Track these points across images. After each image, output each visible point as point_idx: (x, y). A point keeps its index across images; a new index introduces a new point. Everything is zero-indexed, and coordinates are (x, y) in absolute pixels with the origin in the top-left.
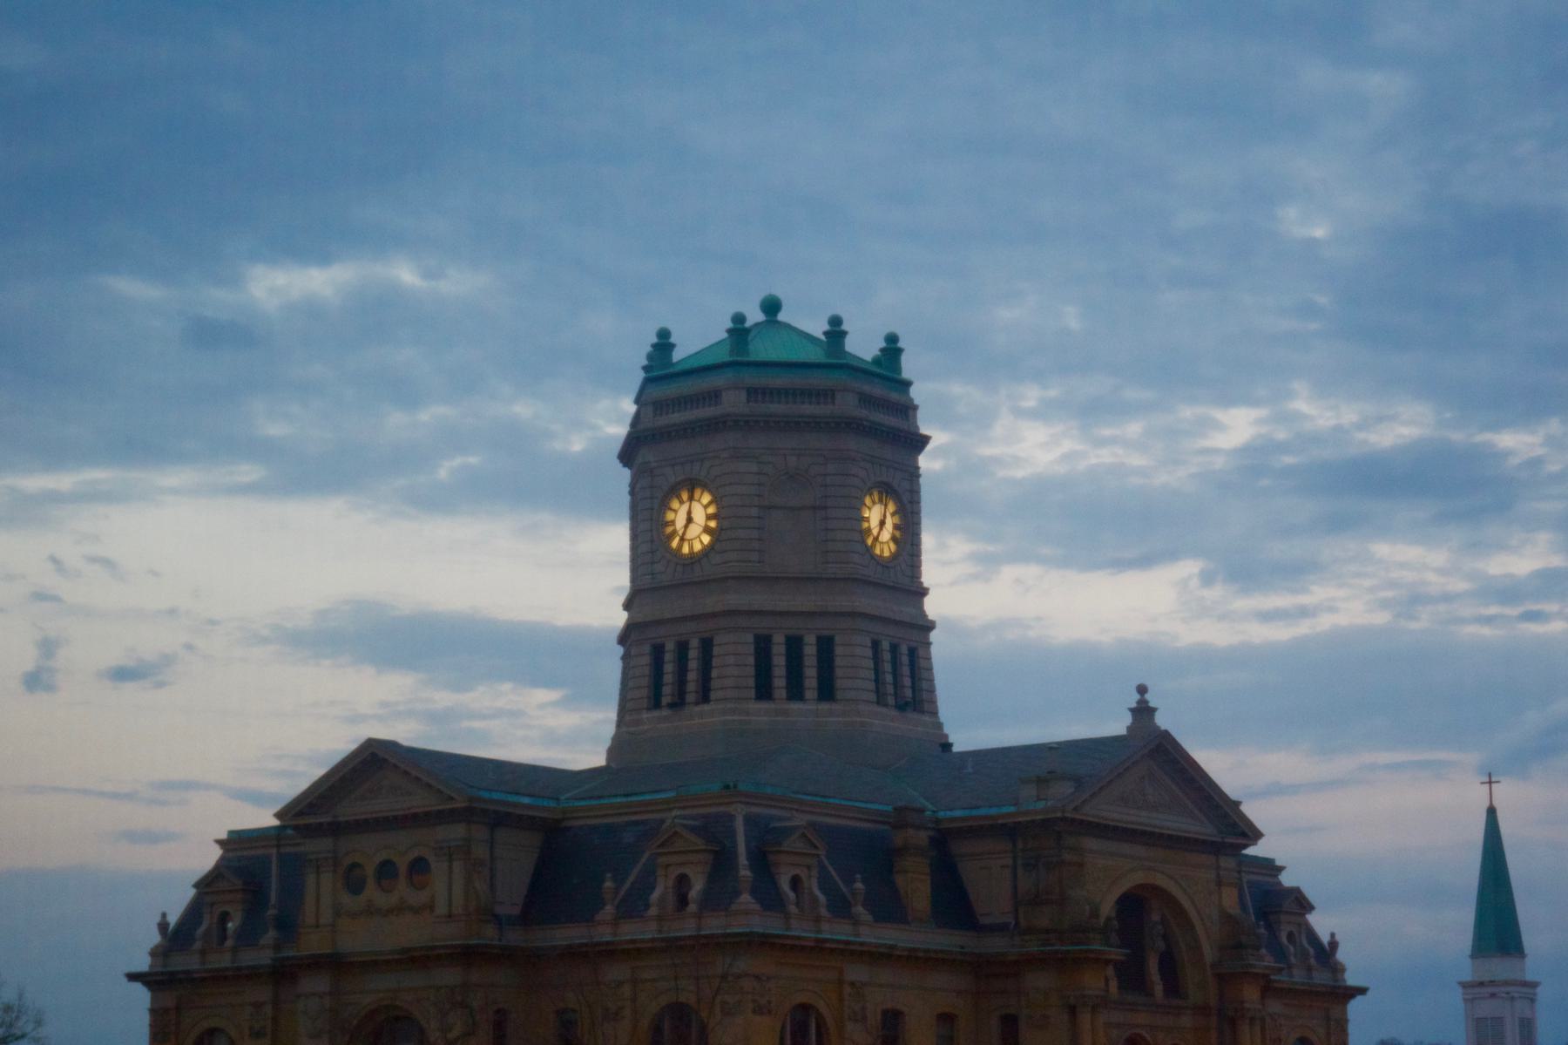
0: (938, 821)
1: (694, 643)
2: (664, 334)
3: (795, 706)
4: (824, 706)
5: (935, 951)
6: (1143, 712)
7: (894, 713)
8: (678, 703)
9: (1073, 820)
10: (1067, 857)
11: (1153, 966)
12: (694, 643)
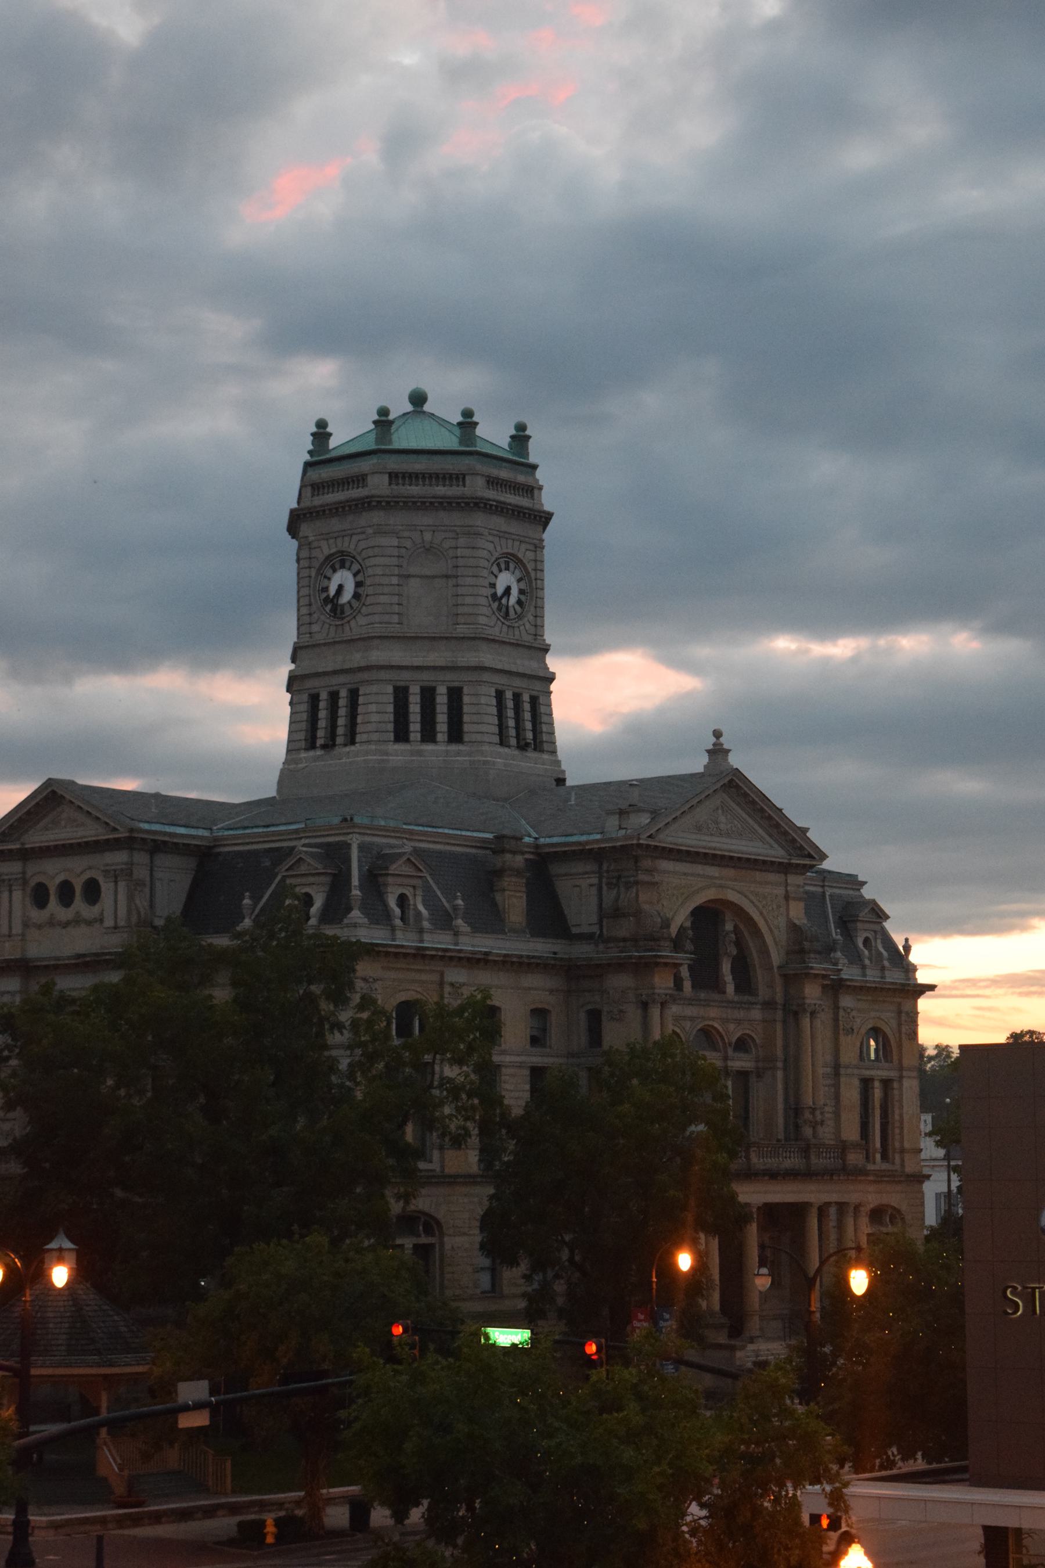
0: (537, 846)
1: (343, 693)
2: (322, 424)
3: (429, 747)
4: (454, 747)
5: (528, 957)
6: (718, 752)
7: (517, 752)
8: (329, 745)
9: (648, 846)
10: (642, 877)
11: (726, 967)
12: (343, 693)
